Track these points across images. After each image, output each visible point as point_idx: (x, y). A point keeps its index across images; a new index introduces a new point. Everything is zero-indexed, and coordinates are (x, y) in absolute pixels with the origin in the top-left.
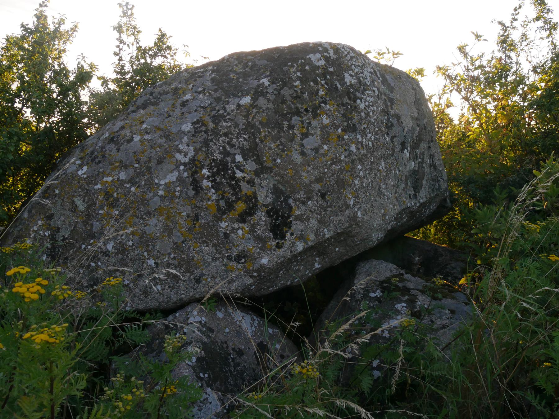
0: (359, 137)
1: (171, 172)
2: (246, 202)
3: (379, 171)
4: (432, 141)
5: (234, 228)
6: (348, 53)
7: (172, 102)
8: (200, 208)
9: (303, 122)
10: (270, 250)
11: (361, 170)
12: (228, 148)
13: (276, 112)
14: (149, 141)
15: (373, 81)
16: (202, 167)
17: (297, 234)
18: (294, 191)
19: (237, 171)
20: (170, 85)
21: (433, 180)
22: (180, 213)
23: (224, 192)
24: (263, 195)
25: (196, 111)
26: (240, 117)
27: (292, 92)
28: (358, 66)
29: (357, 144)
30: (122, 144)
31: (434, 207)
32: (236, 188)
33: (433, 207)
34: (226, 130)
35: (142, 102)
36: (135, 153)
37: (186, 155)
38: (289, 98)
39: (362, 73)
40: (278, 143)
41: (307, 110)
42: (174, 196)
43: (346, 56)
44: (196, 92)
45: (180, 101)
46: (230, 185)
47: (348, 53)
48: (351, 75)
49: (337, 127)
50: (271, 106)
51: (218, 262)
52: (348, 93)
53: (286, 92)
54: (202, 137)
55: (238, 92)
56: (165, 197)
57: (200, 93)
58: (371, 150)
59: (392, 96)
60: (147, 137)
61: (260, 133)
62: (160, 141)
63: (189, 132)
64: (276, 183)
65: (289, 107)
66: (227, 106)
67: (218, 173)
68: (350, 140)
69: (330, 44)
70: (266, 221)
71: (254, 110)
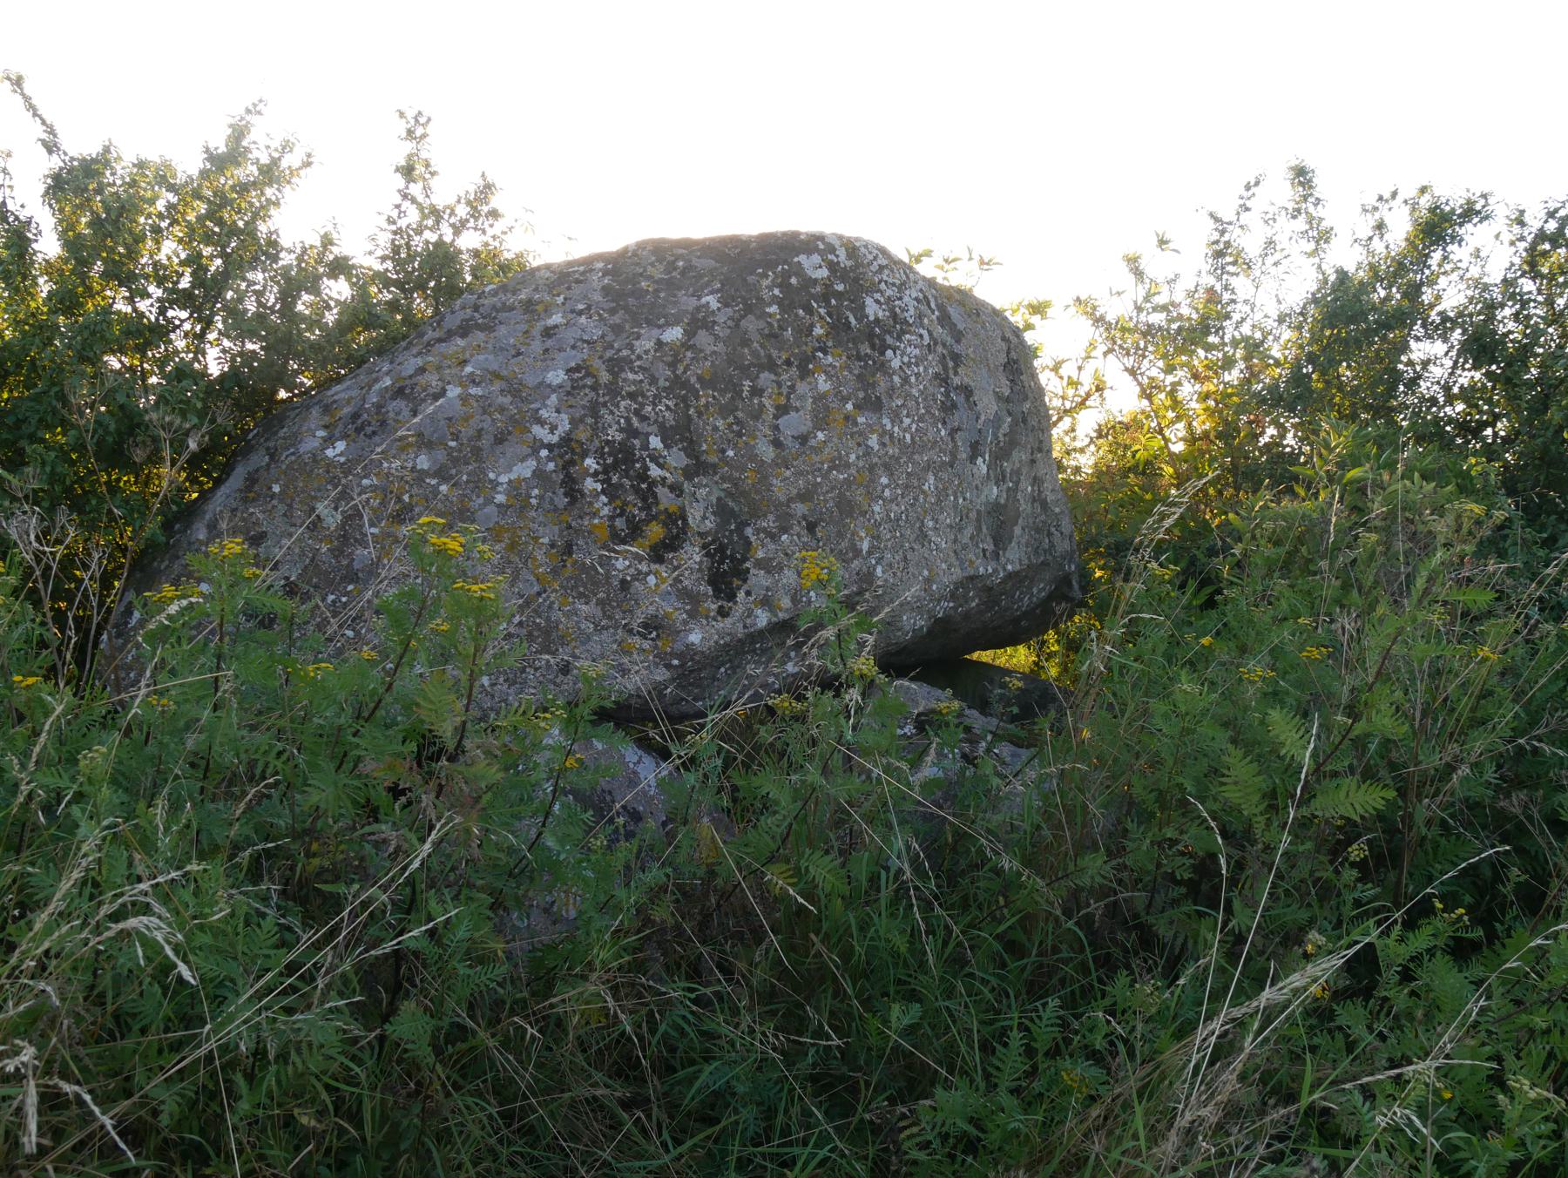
0: (886, 421)
1: (522, 461)
2: (665, 525)
3: (924, 492)
4: (1040, 450)
5: (640, 572)
6: (875, 258)
7: (525, 327)
8: (576, 531)
9: (779, 385)
10: (707, 618)
11: (887, 486)
12: (635, 422)
13: (730, 362)
14: (478, 398)
15: (920, 316)
16: (584, 455)
17: (759, 593)
18: (756, 513)
19: (652, 466)
20: (514, 293)
21: (1038, 530)
22: (536, 539)
23: (625, 504)
24: (698, 516)
25: (573, 347)
26: (661, 365)
27: (761, 324)
28: (894, 284)
29: (881, 436)
30: (424, 400)
31: (1040, 591)
32: (648, 497)
33: (1040, 590)
34: (633, 388)
35: (458, 322)
36: (450, 419)
37: (553, 429)
38: (755, 337)
39: (900, 299)
40: (731, 419)
41: (788, 363)
42: (525, 506)
43: (870, 264)
44: (572, 311)
45: (540, 326)
46: (637, 490)
47: (875, 258)
48: (877, 302)
49: (845, 400)
50: (720, 348)
51: (605, 636)
52: (871, 336)
53: (751, 325)
54: (585, 398)
55: (655, 317)
56: (508, 507)
57: (580, 313)
58: (910, 450)
59: (957, 349)
60: (473, 391)
61: (697, 398)
62: (501, 400)
63: (560, 386)
64: (722, 494)
65: (754, 353)
66: (637, 343)
67: (615, 466)
68: (870, 425)
69: (840, 237)
70: (701, 563)
71: (689, 354)
